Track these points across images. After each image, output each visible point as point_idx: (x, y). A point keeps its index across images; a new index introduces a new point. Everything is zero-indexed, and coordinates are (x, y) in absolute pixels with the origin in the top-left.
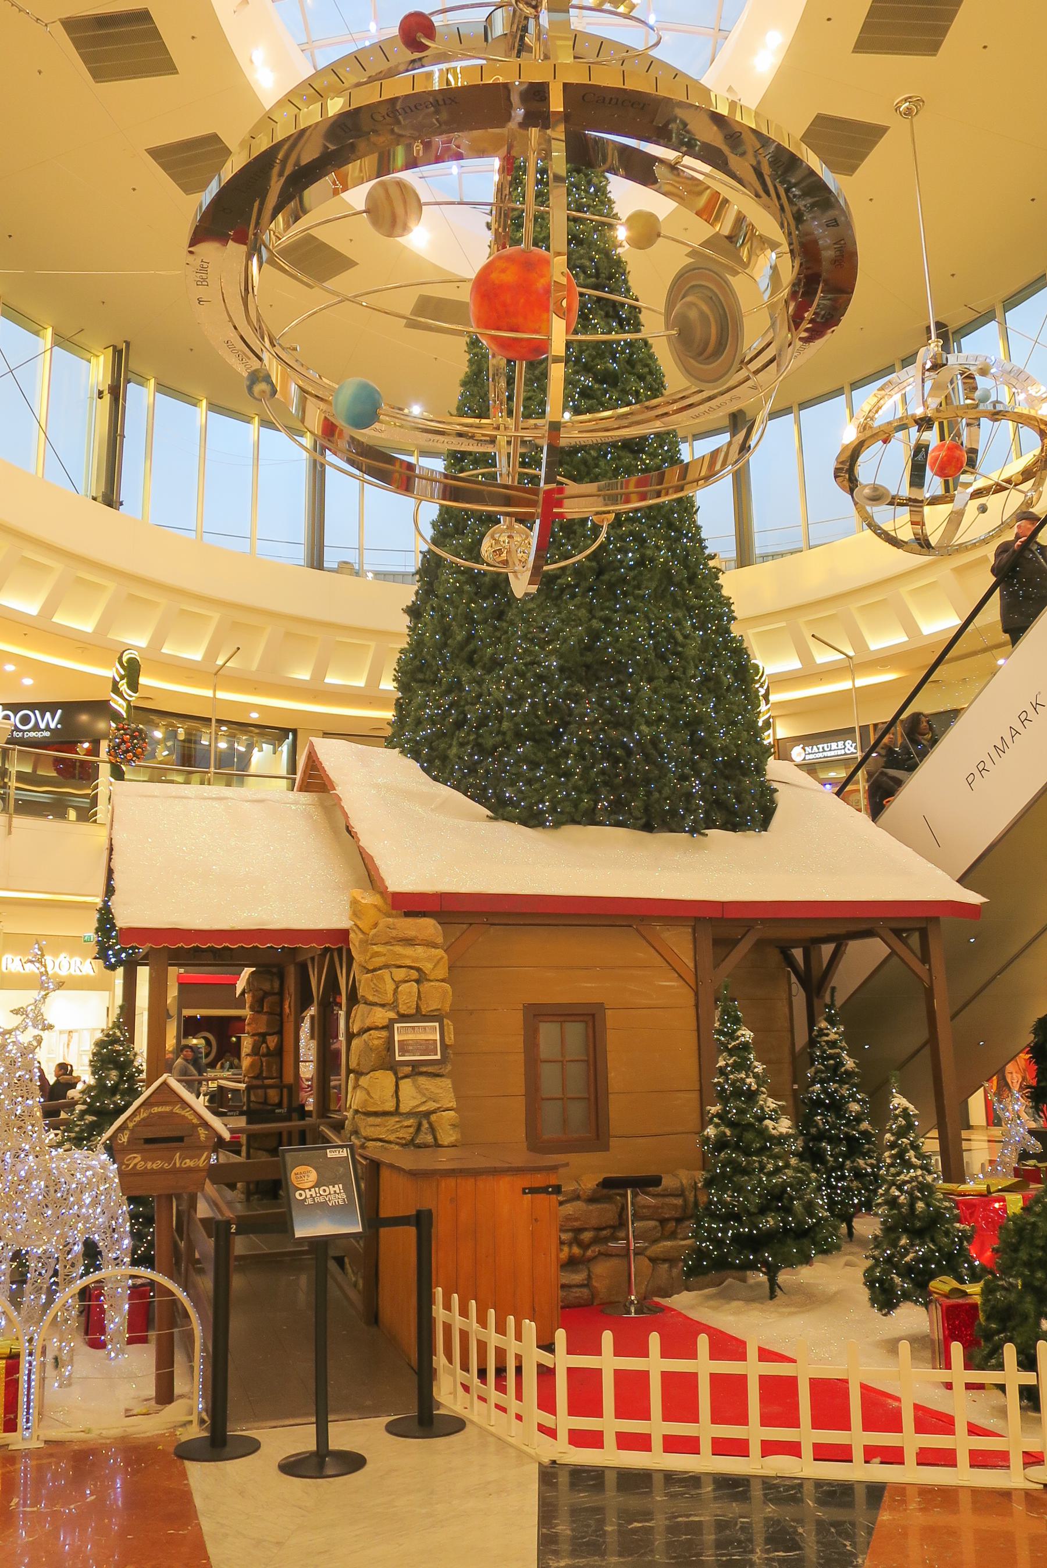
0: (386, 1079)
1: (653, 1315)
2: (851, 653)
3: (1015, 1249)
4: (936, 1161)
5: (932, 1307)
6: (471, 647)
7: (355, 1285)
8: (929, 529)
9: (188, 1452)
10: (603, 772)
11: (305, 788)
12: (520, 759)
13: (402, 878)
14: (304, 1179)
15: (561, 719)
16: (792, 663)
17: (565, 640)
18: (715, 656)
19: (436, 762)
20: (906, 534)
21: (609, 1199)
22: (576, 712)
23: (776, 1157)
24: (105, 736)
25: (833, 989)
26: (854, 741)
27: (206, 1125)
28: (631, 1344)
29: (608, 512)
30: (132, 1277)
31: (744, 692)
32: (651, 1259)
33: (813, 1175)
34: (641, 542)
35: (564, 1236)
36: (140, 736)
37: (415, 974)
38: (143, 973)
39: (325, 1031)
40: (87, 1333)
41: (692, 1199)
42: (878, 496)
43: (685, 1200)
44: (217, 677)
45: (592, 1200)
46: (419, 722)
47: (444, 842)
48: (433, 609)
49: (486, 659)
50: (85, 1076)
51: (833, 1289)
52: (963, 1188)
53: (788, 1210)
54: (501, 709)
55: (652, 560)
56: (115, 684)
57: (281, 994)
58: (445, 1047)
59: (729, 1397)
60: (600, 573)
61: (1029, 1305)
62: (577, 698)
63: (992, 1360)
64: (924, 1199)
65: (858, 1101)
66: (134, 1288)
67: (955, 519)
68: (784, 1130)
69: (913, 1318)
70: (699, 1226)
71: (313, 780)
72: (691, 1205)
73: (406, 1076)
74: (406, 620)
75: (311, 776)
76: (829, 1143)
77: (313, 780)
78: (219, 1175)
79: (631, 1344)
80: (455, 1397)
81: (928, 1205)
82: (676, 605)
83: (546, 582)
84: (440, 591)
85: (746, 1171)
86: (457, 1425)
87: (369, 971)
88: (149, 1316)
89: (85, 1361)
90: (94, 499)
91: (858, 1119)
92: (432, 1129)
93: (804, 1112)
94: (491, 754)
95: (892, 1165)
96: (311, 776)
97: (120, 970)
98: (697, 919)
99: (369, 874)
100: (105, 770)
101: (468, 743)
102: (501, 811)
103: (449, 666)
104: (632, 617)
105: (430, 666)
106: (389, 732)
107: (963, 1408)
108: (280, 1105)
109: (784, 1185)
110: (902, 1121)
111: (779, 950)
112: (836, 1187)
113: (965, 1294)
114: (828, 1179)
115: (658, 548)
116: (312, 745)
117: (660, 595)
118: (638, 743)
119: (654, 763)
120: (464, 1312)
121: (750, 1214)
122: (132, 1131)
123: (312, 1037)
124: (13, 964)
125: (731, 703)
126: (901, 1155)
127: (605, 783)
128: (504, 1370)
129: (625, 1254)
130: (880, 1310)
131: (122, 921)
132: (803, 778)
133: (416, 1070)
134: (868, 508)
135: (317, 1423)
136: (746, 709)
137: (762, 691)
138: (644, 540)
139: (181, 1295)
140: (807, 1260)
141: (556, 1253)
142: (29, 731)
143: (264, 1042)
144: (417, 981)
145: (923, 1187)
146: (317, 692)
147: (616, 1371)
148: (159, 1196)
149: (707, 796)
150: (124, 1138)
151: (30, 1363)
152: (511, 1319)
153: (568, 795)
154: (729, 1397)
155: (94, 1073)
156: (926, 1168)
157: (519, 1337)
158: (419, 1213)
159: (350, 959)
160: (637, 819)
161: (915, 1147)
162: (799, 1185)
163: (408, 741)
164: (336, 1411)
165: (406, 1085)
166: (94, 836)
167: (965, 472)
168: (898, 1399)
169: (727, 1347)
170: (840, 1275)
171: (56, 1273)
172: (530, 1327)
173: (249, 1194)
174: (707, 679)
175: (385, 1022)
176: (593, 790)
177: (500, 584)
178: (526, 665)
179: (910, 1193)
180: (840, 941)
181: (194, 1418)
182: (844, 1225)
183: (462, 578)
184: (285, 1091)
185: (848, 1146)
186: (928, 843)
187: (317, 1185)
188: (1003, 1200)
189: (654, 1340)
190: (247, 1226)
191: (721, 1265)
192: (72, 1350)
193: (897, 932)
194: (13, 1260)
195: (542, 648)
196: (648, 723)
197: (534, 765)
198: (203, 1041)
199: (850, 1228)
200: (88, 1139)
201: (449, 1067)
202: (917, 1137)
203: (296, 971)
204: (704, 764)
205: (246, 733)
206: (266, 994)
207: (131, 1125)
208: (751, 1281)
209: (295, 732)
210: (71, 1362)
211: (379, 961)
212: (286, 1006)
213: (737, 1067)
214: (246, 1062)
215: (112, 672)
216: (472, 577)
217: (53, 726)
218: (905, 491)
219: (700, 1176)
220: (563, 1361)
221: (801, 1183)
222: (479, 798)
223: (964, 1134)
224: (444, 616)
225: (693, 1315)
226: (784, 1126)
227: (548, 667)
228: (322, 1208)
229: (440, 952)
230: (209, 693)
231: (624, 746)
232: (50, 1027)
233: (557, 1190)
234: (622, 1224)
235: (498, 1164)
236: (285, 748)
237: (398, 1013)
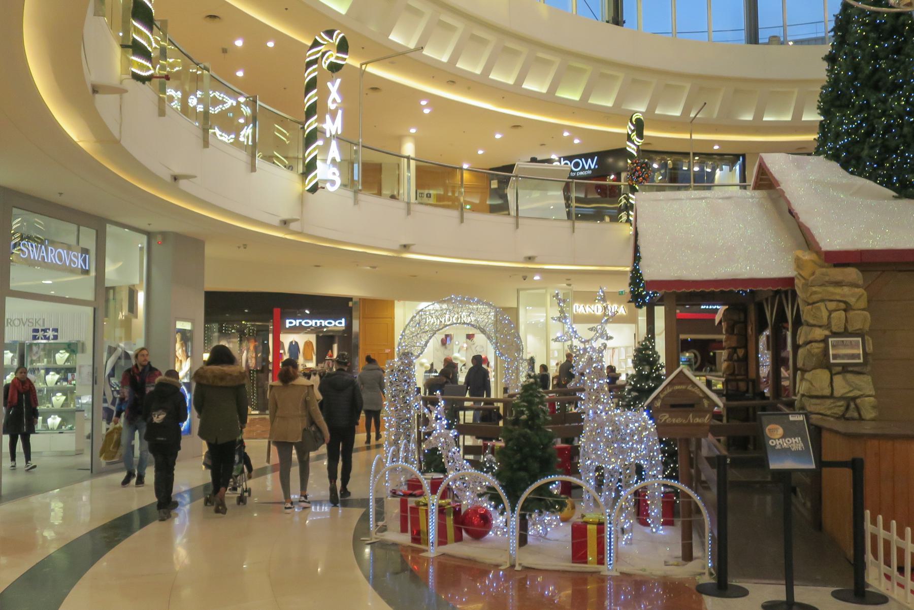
0: (824, 375)
6: (876, 77)
7: (804, 504)
9: (702, 589)
11: (757, 187)
13: (832, 239)
14: (775, 435)
19: (850, 160)
24: (625, 170)
27: (708, 397)
30: (665, 486)
36: (647, 166)
37: (843, 306)
38: (660, 311)
39: (777, 345)
46: (838, 136)
48: (846, 54)
54: (902, 118)
56: (629, 136)
57: (745, 323)
58: (865, 354)
71: (766, 181)
74: (825, 65)
80: (880, 582)
87: (809, 304)
90: (608, 22)
92: (857, 408)
97: (645, 308)
99: (806, 239)
101: (876, 146)
103: (860, 93)
106: (816, 145)
108: (747, 391)
116: (761, 159)
120: (887, 527)
122: (663, 400)
131: (649, 273)
135: (786, 585)
139: (697, 499)
143: (735, 352)
144: (845, 310)
148: (680, 440)
155: (635, 367)
163: (830, 149)
165: (838, 380)
175: (822, 337)
183: (868, 28)
184: (750, 384)
187: (784, 437)
190: (735, 463)
192: (632, 525)
200: (634, 405)
201: (869, 368)
203: (756, 308)
205: (710, 159)
207: (662, 396)
210: (631, 531)
211: (815, 297)
217: (592, 167)
222: (889, 185)
224: (854, 58)
228: (786, 452)
229: (860, 291)
230: (687, 136)
232: (611, 338)
237: (831, 331)
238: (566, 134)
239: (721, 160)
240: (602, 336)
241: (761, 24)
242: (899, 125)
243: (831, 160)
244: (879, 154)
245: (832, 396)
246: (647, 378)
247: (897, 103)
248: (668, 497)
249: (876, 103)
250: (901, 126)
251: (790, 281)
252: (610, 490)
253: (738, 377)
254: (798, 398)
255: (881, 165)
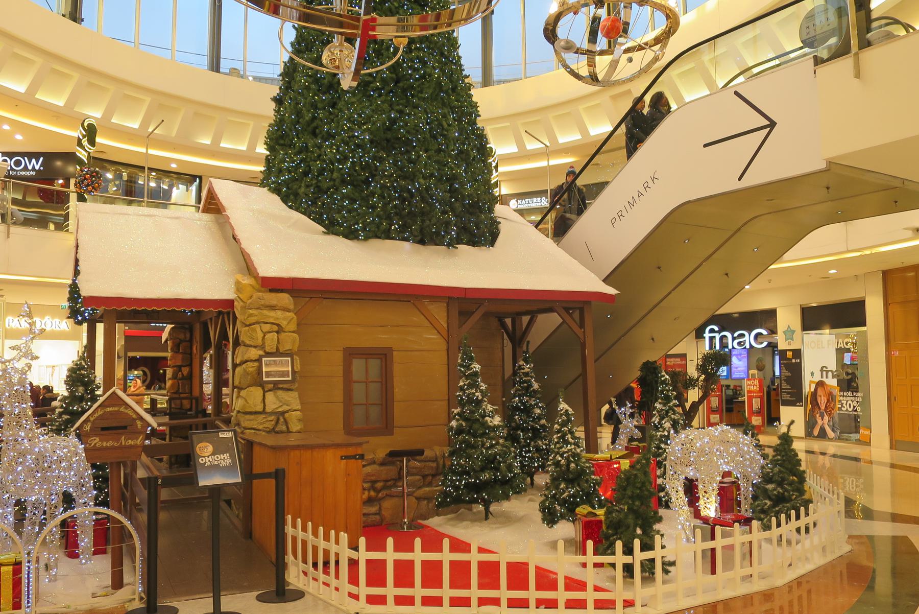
0: (257, 392)
1: (417, 529)
2: (548, 144)
3: (625, 489)
4: (583, 444)
5: (577, 523)
6: (315, 124)
7: (238, 516)
8: (598, 70)
10: (395, 206)
11: (206, 210)
12: (344, 196)
13: (269, 267)
14: (205, 452)
15: (370, 173)
16: (512, 149)
17: (374, 123)
18: (466, 138)
19: (290, 196)
20: (584, 72)
21: (393, 463)
22: (380, 168)
23: (492, 439)
24: (74, 176)
25: (528, 342)
26: (547, 198)
27: (141, 419)
28: (404, 545)
29: (404, 37)
30: (96, 513)
31: (483, 162)
32: (417, 498)
33: (513, 449)
34: (424, 63)
35: (366, 485)
36: (97, 175)
37: (276, 328)
38: (100, 328)
39: (219, 367)
40: (66, 548)
41: (441, 462)
42: (569, 47)
43: (438, 464)
44: (148, 139)
45: (382, 464)
46: (280, 171)
47: (293, 246)
48: (291, 99)
49: (324, 133)
50: (61, 390)
51: (522, 513)
52: (597, 456)
53: (497, 469)
54: (333, 165)
55: (430, 75)
56: (79, 141)
57: (191, 341)
59: (460, 574)
60: (397, 82)
61: (630, 520)
62: (381, 160)
63: (609, 550)
64: (575, 462)
65: (540, 408)
66: (96, 521)
67: (614, 65)
68: (496, 423)
69: (566, 529)
70: (446, 479)
71: (211, 205)
72: (441, 466)
73: (268, 388)
74: (273, 105)
75: (210, 204)
76: (522, 431)
77: (211, 205)
78: (150, 451)
79: (404, 545)
81: (577, 465)
82: (444, 105)
83: (364, 85)
84: (295, 88)
85: (473, 447)
86: (299, 595)
87: (246, 326)
88: (106, 537)
89: (66, 566)
90: (64, 16)
91: (539, 418)
93: (508, 413)
94: (326, 193)
95: (558, 443)
96: (210, 204)
97: (85, 325)
98: (449, 298)
99: (248, 267)
100: (73, 197)
102: (331, 229)
103: (300, 136)
104: (417, 111)
105: (288, 136)
106: (261, 176)
107: (591, 577)
108: (190, 410)
109: (496, 454)
110: (564, 418)
111: (497, 317)
112: (525, 457)
113: (595, 515)
114: (521, 452)
115: (434, 68)
117: (434, 98)
118: (417, 190)
119: (427, 203)
120: (304, 529)
121: (475, 471)
123: (211, 368)
124: (14, 323)
125: (475, 168)
126: (563, 437)
127: (397, 214)
128: (328, 563)
129: (401, 495)
130: (548, 525)
131: (87, 290)
132: (517, 216)
133: (276, 386)
134: (563, 54)
136: (484, 173)
137: (494, 164)
138: (425, 63)
139: (127, 523)
140: (507, 498)
141: (359, 495)
142: (21, 170)
143: (180, 370)
144: (277, 332)
145: (575, 455)
146: (214, 152)
147: (395, 561)
148: (112, 463)
149: (459, 224)
150: (88, 427)
151: (29, 567)
152: (333, 532)
153: (374, 220)
154: (460, 574)
156: (577, 445)
157: (337, 542)
158: (277, 471)
159: (235, 318)
160: (415, 236)
161: (572, 433)
162: (504, 454)
164: (225, 590)
166: (65, 240)
167: (621, 36)
168: (556, 574)
169: (459, 546)
170: (525, 506)
171: (45, 513)
172: (344, 536)
173: (171, 465)
174: (461, 152)
175: (257, 357)
176: (389, 218)
177: (333, 83)
178: (349, 137)
179: (567, 459)
180: (533, 314)
181: (137, 597)
182: (529, 479)
183: (310, 80)
185: (533, 434)
186: (587, 258)
187: (213, 454)
188: (619, 463)
189: (418, 542)
190: (168, 482)
191: (458, 501)
192: (56, 559)
193: (567, 310)
194: (16, 505)
195: (360, 127)
196: (424, 178)
197: (353, 201)
198: (141, 373)
199: (532, 480)
200: (65, 430)
201: (297, 385)
202: (572, 427)
203: (199, 328)
204: (457, 205)
205: (168, 177)
206: (181, 341)
207: (92, 419)
208: (475, 510)
209: (200, 178)
212: (194, 349)
213: (470, 386)
214: (169, 383)
215: (77, 133)
216: (315, 78)
217: (37, 168)
218: (585, 46)
219: (447, 450)
220: (364, 555)
221: (505, 453)
222: (318, 220)
223: (599, 429)
224: (297, 104)
225: (441, 530)
226: (497, 420)
227: (363, 140)
228: (215, 468)
229: (292, 315)
230: (143, 150)
231: (409, 191)
232: (37, 358)
233: (362, 457)
234: (400, 477)
235: (326, 442)
236: (194, 188)
238: (6, 127)
239: (178, 179)
240: (26, 355)
241: (223, 54)
242: (330, 170)
243: (273, 192)
244: (313, 193)
245: (264, 412)
246: (81, 399)
247: (330, 150)
248: (102, 524)
249: (313, 148)
250: (332, 171)
251: (230, 303)
252: (34, 524)
253: (182, 395)
254: (234, 414)
255: (314, 203)
